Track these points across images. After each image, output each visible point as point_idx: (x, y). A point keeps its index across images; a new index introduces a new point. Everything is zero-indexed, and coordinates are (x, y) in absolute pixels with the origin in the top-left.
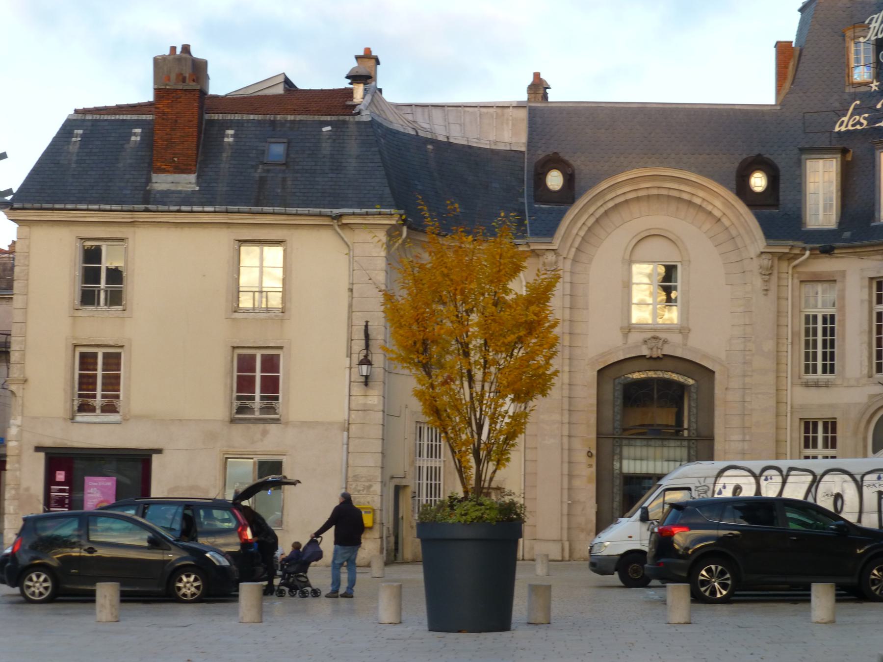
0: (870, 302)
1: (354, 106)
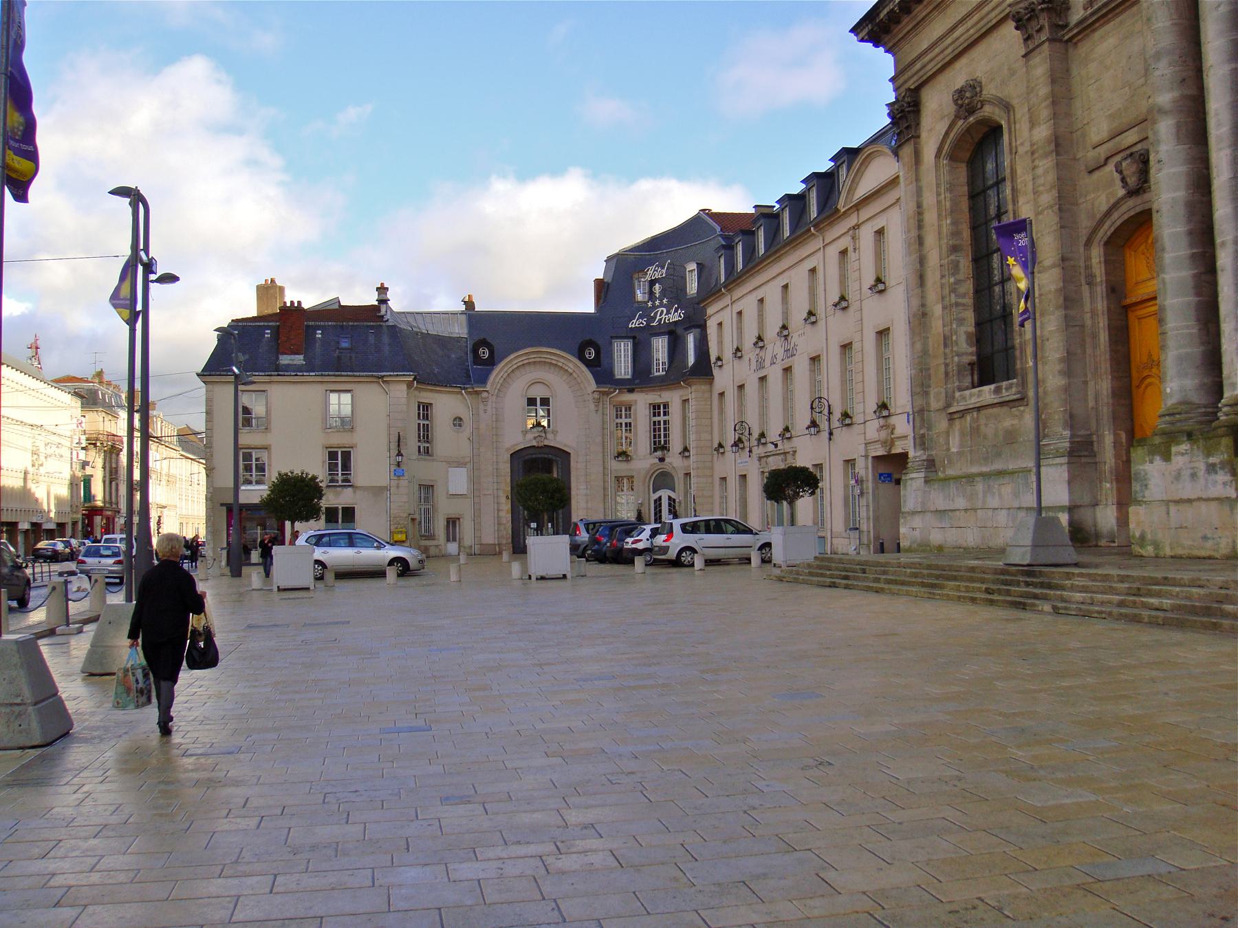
1: (383, 316)
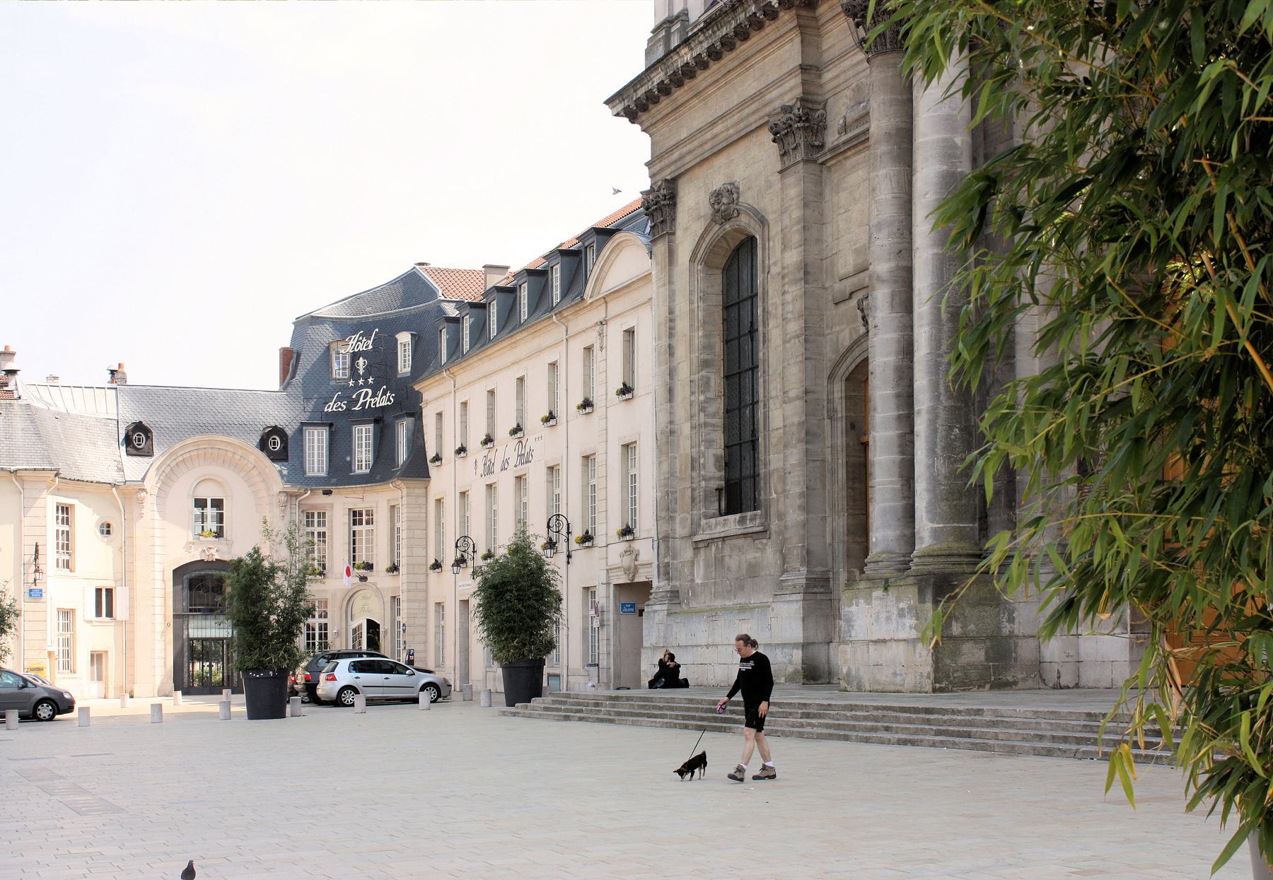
0: (349, 524)
